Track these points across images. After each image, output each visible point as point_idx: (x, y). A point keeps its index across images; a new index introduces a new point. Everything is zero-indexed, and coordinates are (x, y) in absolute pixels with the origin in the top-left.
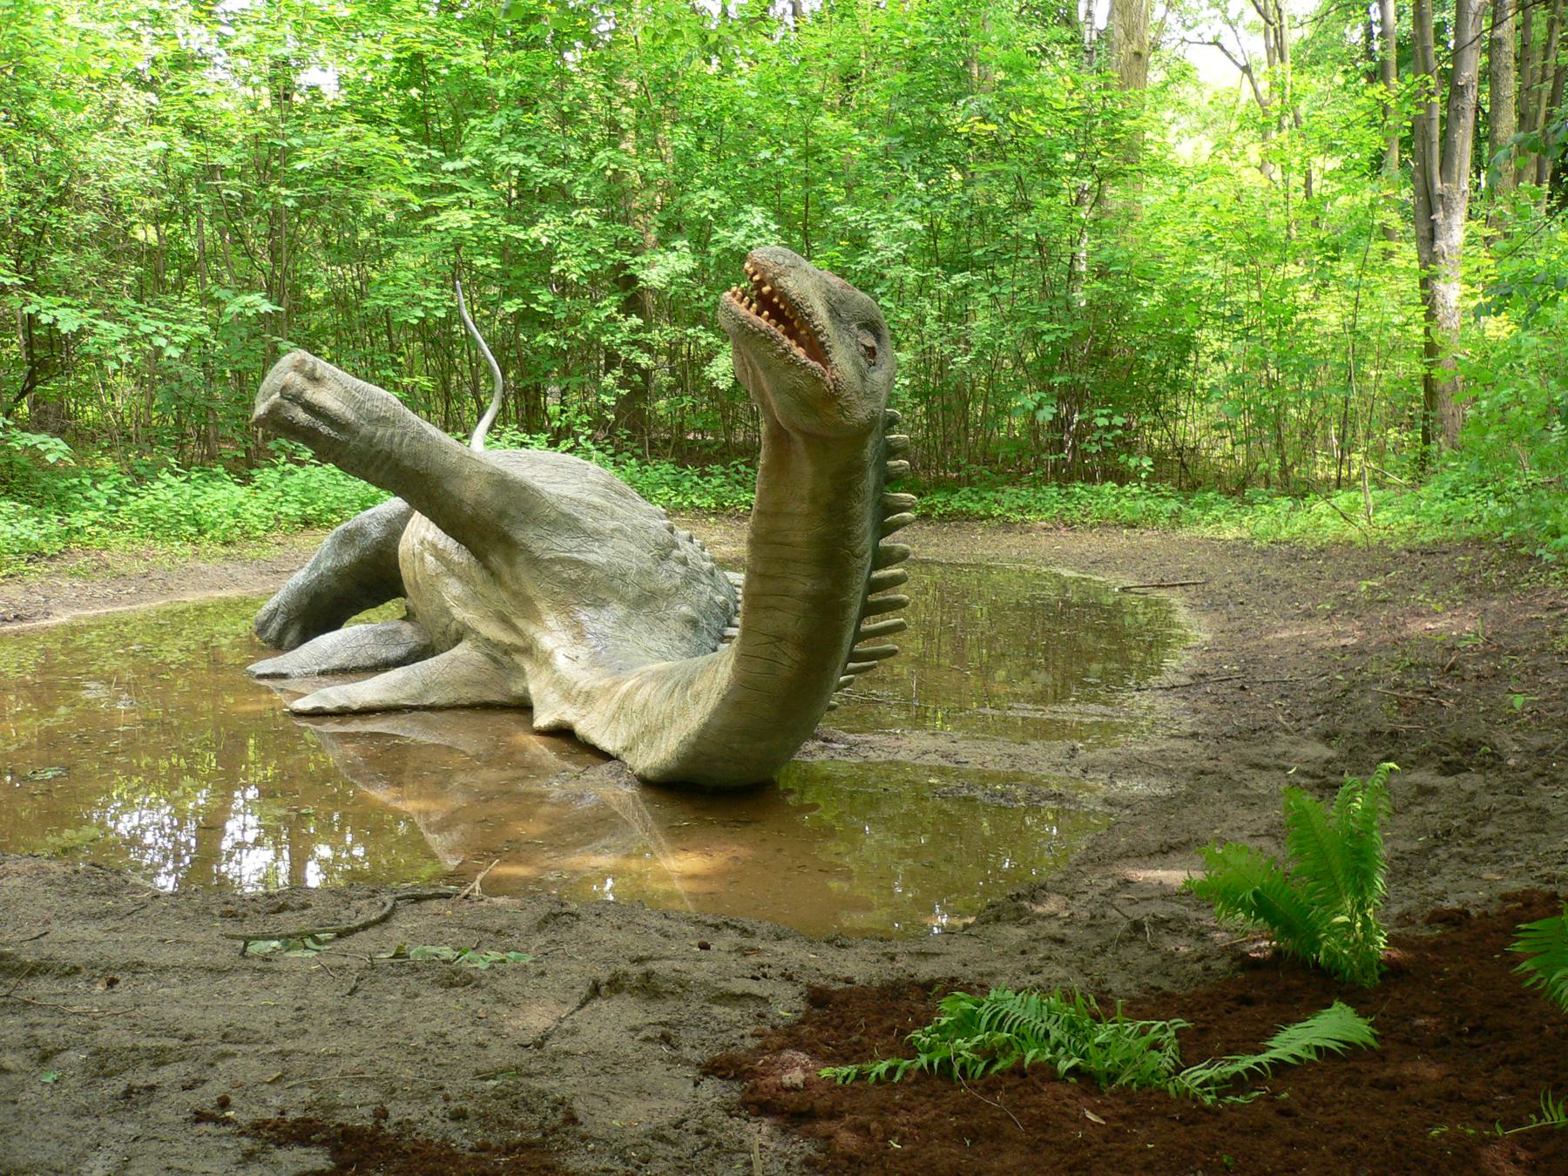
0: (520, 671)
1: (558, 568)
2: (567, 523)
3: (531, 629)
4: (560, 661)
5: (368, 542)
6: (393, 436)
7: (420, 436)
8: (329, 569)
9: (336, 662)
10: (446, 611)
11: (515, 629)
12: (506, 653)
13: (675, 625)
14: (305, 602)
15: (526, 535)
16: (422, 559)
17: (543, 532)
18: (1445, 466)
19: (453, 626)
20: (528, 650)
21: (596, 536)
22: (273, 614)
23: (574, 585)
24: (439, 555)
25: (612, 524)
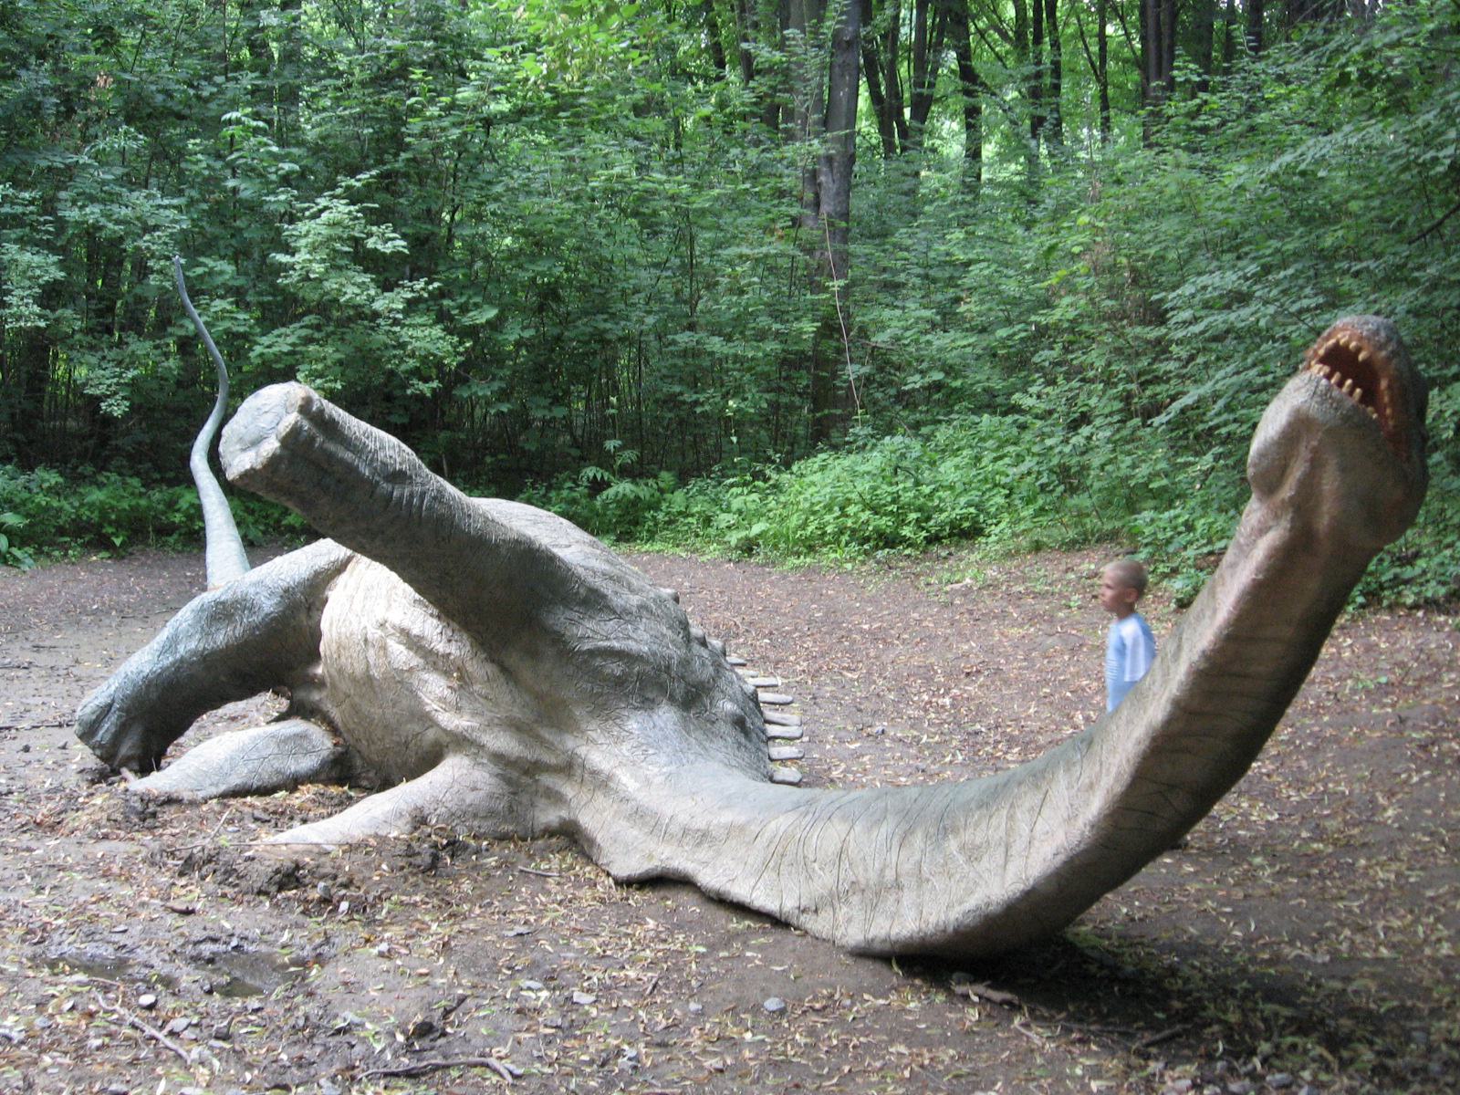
0: (556, 798)
1: (598, 662)
2: (594, 602)
3: (570, 742)
4: (627, 781)
5: (256, 619)
6: (411, 495)
7: (439, 496)
8: (194, 653)
9: (235, 781)
10: (427, 719)
11: (542, 742)
12: (526, 773)
13: (725, 728)
14: (154, 696)
15: (560, 619)
16: (384, 648)
17: (575, 616)
18: (1029, 450)
19: (431, 735)
20: (569, 768)
21: (622, 614)
22: (106, 710)
23: (620, 682)
24: (414, 643)
25: (635, 600)
